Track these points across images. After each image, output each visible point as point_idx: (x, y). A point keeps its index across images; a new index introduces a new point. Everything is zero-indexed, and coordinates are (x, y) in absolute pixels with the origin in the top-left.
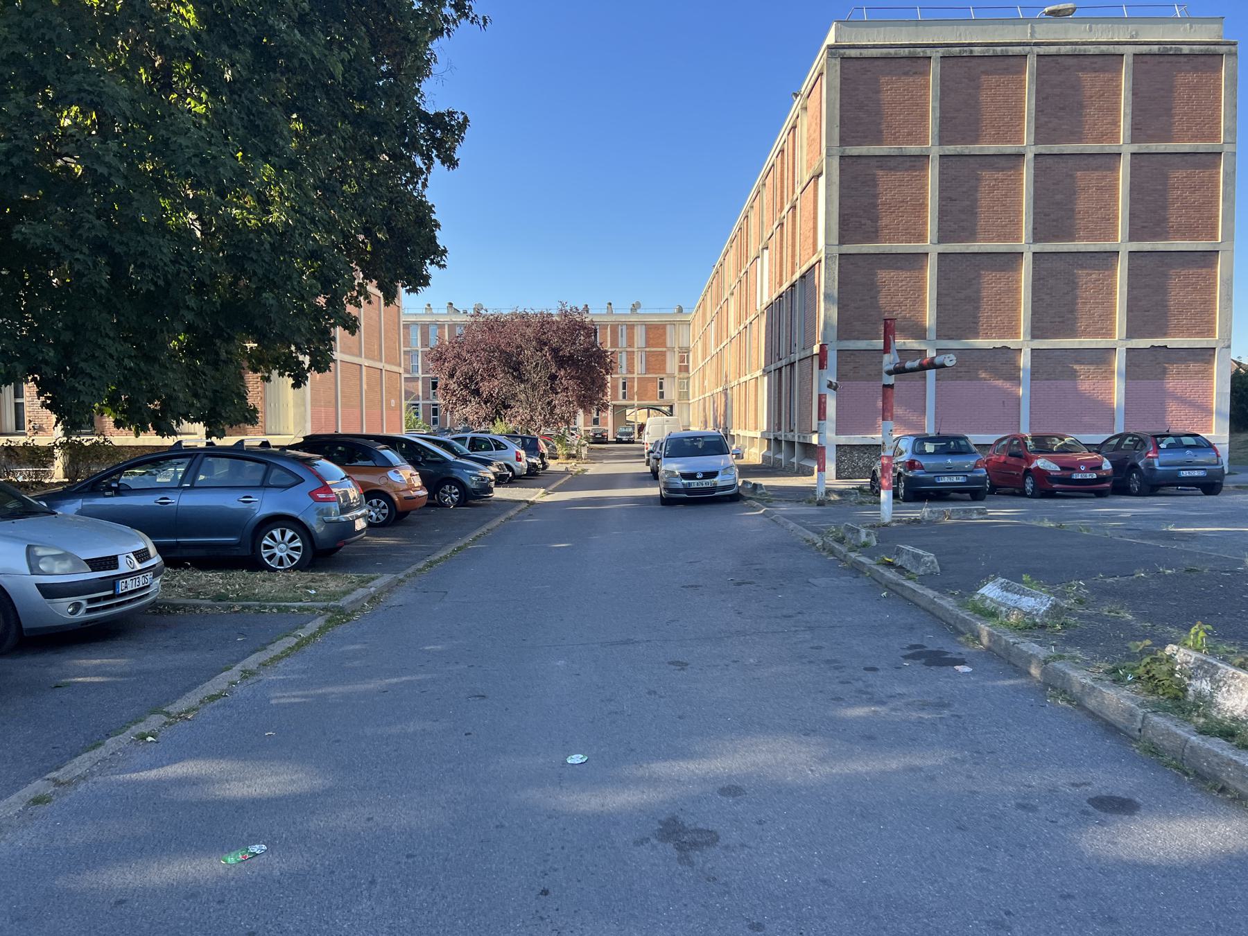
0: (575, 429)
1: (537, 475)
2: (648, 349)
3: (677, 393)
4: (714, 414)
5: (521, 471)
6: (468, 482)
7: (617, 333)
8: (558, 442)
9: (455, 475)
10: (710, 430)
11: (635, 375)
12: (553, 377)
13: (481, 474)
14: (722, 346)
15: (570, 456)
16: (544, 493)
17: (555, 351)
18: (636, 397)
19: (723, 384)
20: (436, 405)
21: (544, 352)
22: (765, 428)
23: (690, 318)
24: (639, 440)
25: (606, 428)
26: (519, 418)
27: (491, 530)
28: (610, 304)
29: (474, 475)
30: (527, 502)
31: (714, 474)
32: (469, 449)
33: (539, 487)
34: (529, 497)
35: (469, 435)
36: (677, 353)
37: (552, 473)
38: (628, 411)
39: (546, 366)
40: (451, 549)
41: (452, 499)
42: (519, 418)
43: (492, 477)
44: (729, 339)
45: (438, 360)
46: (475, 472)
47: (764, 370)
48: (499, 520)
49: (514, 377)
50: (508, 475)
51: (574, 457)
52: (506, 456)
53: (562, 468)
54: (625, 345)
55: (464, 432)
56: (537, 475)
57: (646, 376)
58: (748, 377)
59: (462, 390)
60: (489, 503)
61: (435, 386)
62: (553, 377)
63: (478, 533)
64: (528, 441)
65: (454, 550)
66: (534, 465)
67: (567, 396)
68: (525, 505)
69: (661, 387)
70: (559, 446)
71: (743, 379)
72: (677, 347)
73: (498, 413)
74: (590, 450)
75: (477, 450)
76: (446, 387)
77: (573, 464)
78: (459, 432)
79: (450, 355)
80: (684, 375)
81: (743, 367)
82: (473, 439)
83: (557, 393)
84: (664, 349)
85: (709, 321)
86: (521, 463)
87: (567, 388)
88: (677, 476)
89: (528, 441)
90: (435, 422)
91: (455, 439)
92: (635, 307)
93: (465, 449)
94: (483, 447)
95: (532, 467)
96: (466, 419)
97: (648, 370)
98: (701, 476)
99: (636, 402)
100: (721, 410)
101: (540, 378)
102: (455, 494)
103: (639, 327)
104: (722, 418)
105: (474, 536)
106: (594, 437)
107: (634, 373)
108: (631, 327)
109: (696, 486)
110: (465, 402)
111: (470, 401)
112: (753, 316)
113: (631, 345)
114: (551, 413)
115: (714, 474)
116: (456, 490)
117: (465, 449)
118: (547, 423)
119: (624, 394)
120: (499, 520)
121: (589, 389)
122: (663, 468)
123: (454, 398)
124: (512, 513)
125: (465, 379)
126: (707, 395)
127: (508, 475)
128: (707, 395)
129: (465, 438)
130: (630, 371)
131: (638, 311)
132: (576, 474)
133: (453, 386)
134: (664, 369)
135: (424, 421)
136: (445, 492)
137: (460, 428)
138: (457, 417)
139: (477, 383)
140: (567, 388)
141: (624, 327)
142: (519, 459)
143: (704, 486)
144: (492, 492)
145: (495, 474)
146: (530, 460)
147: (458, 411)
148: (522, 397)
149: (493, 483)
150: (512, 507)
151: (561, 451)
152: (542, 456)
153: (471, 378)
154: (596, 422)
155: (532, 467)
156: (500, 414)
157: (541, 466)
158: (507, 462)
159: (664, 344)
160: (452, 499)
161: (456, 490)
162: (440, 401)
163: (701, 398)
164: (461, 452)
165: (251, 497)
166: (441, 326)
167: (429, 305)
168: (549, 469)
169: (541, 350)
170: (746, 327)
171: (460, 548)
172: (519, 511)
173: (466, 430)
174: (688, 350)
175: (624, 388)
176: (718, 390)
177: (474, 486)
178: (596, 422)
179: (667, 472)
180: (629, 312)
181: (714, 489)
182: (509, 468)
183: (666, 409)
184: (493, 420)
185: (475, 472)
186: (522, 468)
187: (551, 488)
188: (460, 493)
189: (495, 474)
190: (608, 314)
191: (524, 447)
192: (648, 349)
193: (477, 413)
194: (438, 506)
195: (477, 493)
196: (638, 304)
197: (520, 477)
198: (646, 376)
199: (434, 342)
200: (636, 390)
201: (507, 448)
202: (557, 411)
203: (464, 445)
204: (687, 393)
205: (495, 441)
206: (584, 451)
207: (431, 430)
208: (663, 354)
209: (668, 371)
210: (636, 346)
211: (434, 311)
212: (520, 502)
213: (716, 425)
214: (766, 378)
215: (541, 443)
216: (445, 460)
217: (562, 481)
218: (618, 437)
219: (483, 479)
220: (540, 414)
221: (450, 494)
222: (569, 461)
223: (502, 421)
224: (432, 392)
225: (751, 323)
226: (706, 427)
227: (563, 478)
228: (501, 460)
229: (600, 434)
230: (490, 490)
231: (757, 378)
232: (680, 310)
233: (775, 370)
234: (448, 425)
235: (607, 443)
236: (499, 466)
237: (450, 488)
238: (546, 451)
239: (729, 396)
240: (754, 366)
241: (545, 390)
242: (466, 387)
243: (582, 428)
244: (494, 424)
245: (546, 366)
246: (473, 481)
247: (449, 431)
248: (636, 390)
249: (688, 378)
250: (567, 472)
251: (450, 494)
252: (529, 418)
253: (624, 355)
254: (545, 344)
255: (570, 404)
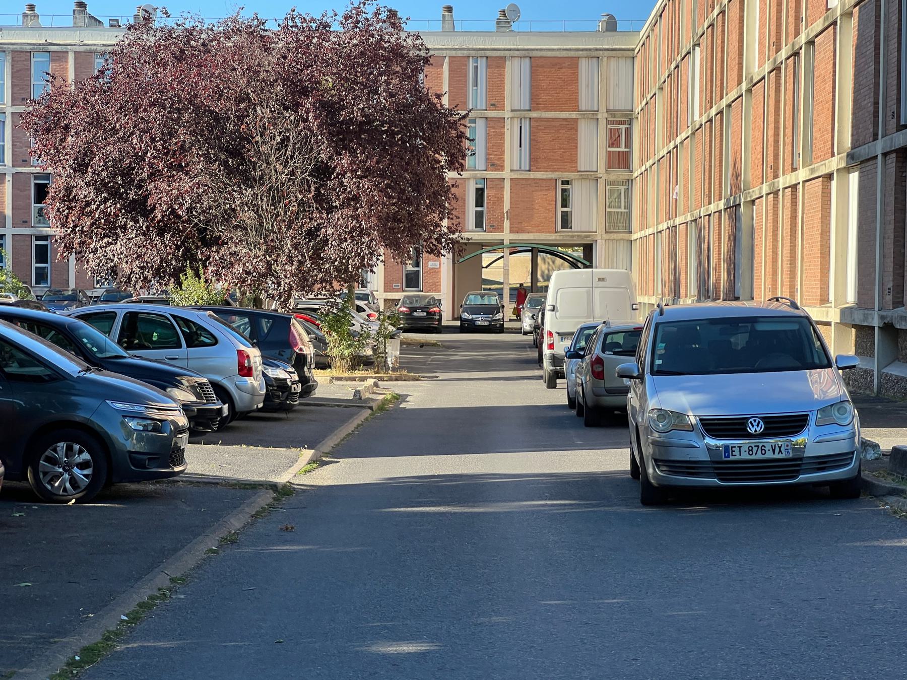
0: (365, 297)
1: (289, 409)
2: (534, 114)
3: (602, 214)
4: (700, 263)
5: (252, 401)
6: (117, 435)
7: (466, 75)
8: (331, 327)
9: (81, 415)
10: (689, 301)
11: (506, 174)
12: (323, 172)
13: (156, 415)
14: (724, 103)
15: (358, 362)
16: (312, 461)
17: (329, 109)
18: (507, 224)
19: (726, 191)
20: (45, 238)
21: (301, 112)
22: (851, 297)
23: (634, 43)
24: (516, 325)
25: (436, 296)
26: (239, 269)
27: (183, 580)
28: (449, 9)
29: (134, 416)
30: (274, 487)
31: (796, 423)
32: (120, 343)
33: (299, 443)
34: (275, 471)
35: (121, 308)
36: (602, 123)
37: (323, 403)
38: (487, 259)
39: (306, 145)
40: (63, 659)
41: (73, 481)
42: (239, 269)
43: (183, 421)
44: (744, 86)
45: (48, 130)
46: (137, 408)
47: (851, 156)
48: (203, 548)
49: (230, 171)
50: (220, 411)
51: (367, 363)
52: (211, 363)
53: (344, 391)
54: (481, 104)
55: (107, 301)
56: (289, 409)
57: (532, 175)
58: (802, 174)
59: (106, 200)
60: (170, 489)
61: (41, 193)
62: (323, 172)
63: (144, 593)
64: (265, 325)
65: (72, 663)
66: (282, 385)
67: (356, 218)
68: (267, 497)
69: (565, 204)
70: (332, 338)
71: (783, 181)
72: (602, 109)
73: (189, 256)
74: (406, 346)
75: (141, 347)
76: (68, 196)
77: (371, 382)
78: (97, 300)
79: (77, 118)
80: (619, 174)
81: (784, 151)
82: (132, 319)
83: (330, 210)
84: (574, 115)
85: (686, 46)
86: (250, 380)
87: (356, 198)
88: (692, 428)
89: (265, 325)
90: (41, 276)
91: (85, 317)
92: (506, 19)
93: (111, 344)
94: (155, 337)
95: (277, 388)
96: (114, 271)
97: (535, 162)
98: (760, 429)
99: (506, 236)
100: (719, 248)
101: (292, 173)
102: (83, 466)
103: (516, 62)
104: (724, 267)
105: (132, 607)
106: (409, 316)
107: (501, 168)
108: (496, 62)
109: (745, 456)
110: (112, 230)
111: (124, 228)
112: (818, 25)
113: (496, 105)
114: (316, 257)
115: (796, 423)
116: (86, 456)
117: (111, 344)
118: (305, 284)
119: (479, 217)
120: (203, 548)
121: (409, 202)
122: (652, 404)
123: (87, 222)
124: (236, 523)
125: (114, 176)
126: (678, 221)
127: (220, 411)
128: (678, 221)
129: (111, 316)
130: (495, 163)
131: (515, 26)
132: (381, 408)
133: (84, 192)
134: (573, 160)
135: (15, 273)
136: (53, 461)
137: (99, 292)
138: (92, 264)
139: (140, 187)
140: (356, 198)
141: (482, 63)
142: (245, 371)
143: (769, 455)
144: (180, 461)
145: (186, 408)
146: (273, 373)
147: (95, 251)
148: (248, 217)
149: (185, 436)
150: (234, 505)
151: (337, 349)
152: (300, 362)
153: (127, 173)
154: (412, 280)
155: (277, 388)
156: (193, 259)
157: (298, 388)
158: (217, 378)
159: (573, 103)
160: (73, 481)
161: (86, 456)
162: (55, 230)
163: (663, 226)
164: (101, 350)
165: (799, 154)
166: (59, 56)
167: (31, 7)
168: (318, 393)
169: (297, 106)
170: (796, 54)
171: (90, 654)
172: (255, 516)
173: (112, 297)
174: (628, 118)
175: (479, 202)
176: (713, 208)
177: (132, 445)
178: (412, 280)
179: (662, 414)
180: (493, 27)
181: (796, 463)
182: (223, 393)
183: (579, 253)
184: (176, 274)
185: (137, 408)
186: (253, 392)
187: (330, 443)
188: (94, 463)
189: (186, 408)
190: (444, 32)
191: (256, 339)
192: (534, 114)
193: (139, 256)
194: (36, 500)
195: (140, 464)
196: (515, 10)
197: (240, 415)
198: (532, 175)
199: (39, 88)
200: (507, 206)
201: (215, 341)
202: (330, 252)
203: (108, 332)
204: (628, 216)
205: (187, 322)
206: (393, 351)
207: (32, 297)
208: (571, 126)
209: (583, 165)
210: (508, 107)
211: (42, 21)
212: (254, 486)
213: (704, 292)
214: (854, 178)
215: (298, 328)
216: (57, 375)
217: (350, 427)
218: (466, 316)
219: (158, 426)
220: (290, 260)
221: (68, 468)
222: (358, 374)
223: (197, 275)
224: (35, 206)
225: (811, 43)
226: (676, 295)
227: (351, 416)
228: (200, 372)
229: (423, 309)
230: (177, 456)
231: (829, 176)
232: (611, 25)
233: (885, 155)
234: (72, 285)
235: (439, 330)
236: (195, 389)
237: (70, 449)
238: (309, 350)
239: (744, 220)
240: (821, 145)
241: (301, 203)
242: (115, 194)
243: (381, 296)
244: (180, 284)
245: (306, 145)
246: (130, 433)
247: (73, 299)
248: (507, 206)
249: (630, 182)
250: (358, 403)
251: (68, 468)
252: (262, 268)
253: (480, 125)
254: (305, 92)
255: (361, 235)
